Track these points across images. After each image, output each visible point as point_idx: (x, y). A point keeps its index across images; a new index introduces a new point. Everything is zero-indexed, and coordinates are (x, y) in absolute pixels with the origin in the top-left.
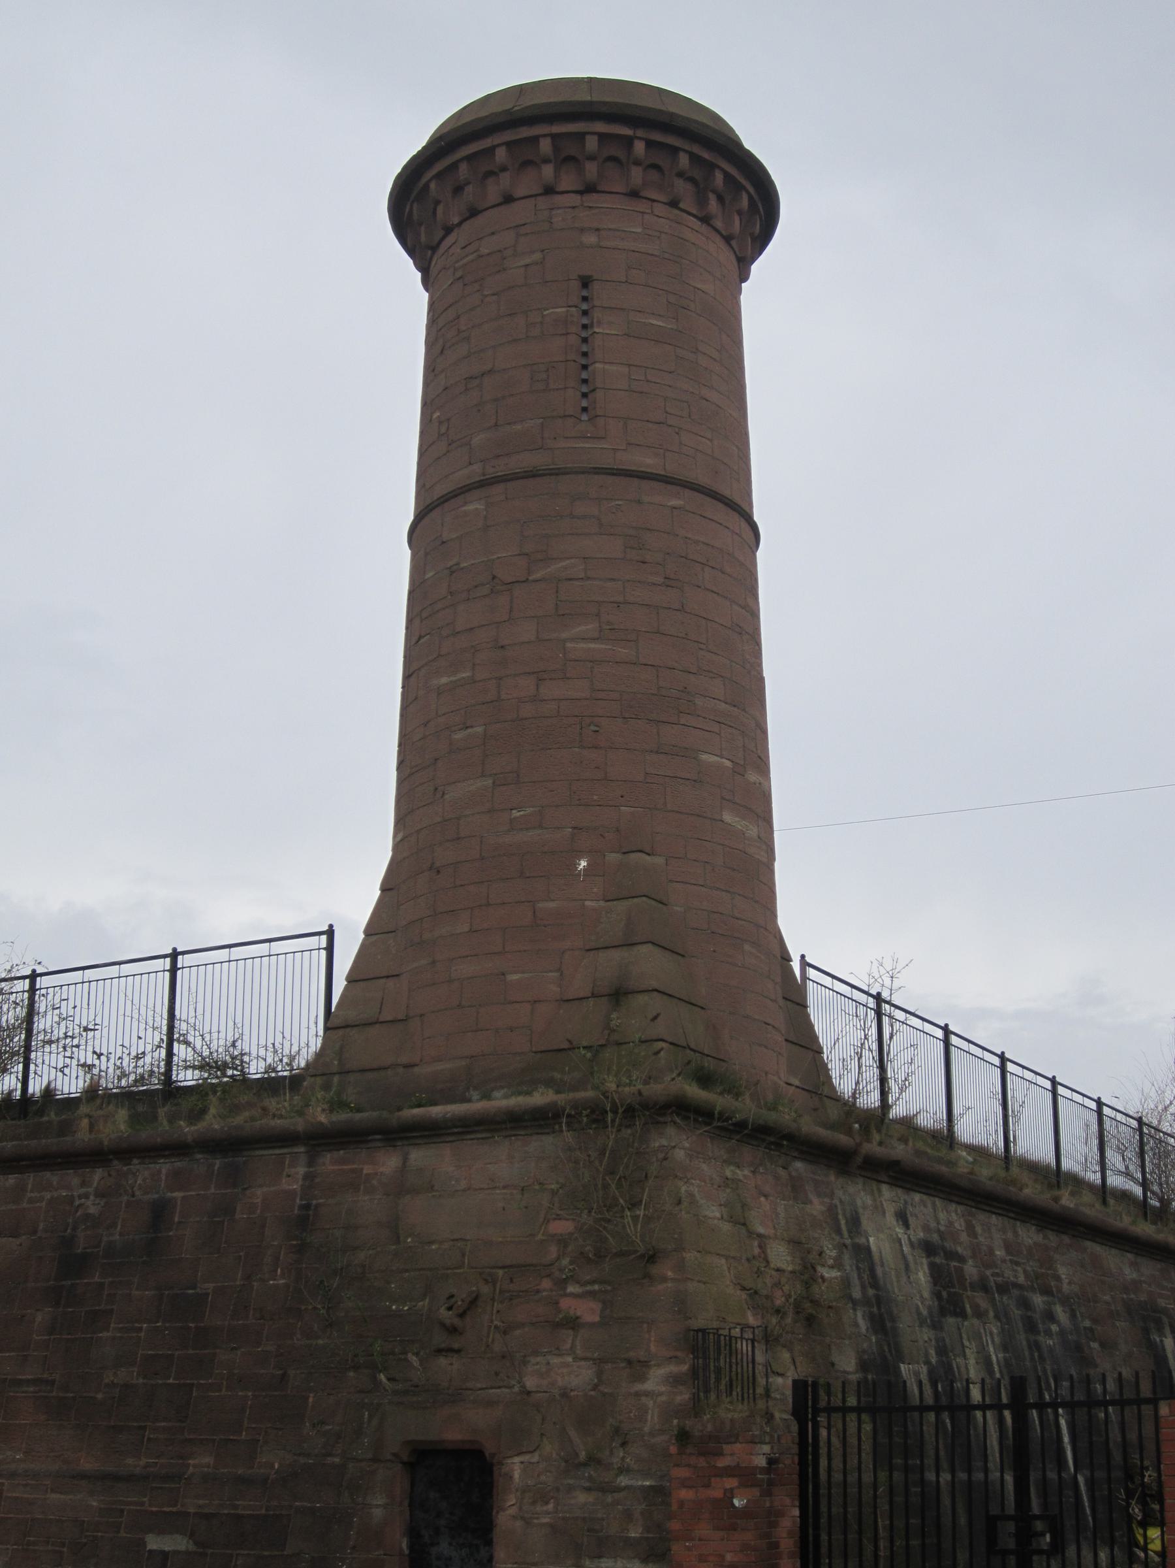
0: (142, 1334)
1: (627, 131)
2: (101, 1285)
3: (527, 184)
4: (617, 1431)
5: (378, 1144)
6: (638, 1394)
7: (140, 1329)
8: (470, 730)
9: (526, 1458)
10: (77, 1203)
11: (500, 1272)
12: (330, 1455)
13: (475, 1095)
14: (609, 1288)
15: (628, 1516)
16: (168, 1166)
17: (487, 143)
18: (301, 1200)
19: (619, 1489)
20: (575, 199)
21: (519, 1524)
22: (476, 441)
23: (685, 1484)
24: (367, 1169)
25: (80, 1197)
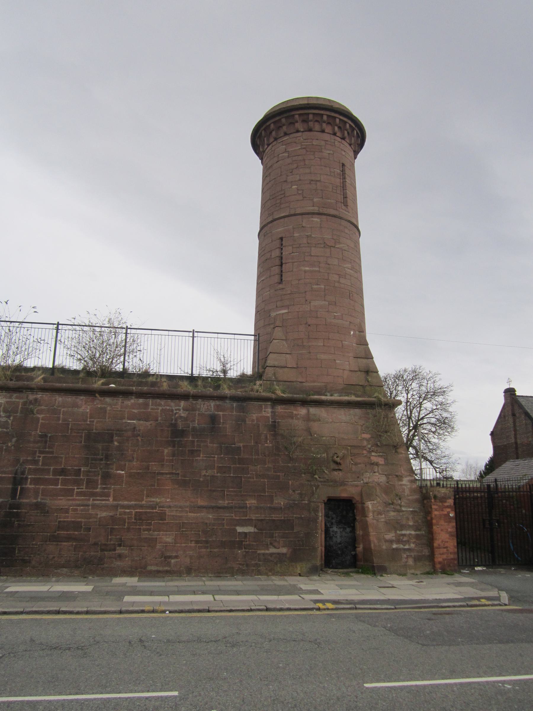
0: (216, 459)
1: (277, 118)
2: (193, 442)
3: (328, 129)
4: (397, 495)
5: (299, 405)
6: (401, 485)
7: (215, 457)
8: (319, 286)
9: (372, 502)
10: (175, 412)
11: (349, 448)
12: (304, 500)
13: (328, 394)
14: (385, 455)
15: (408, 519)
16: (214, 403)
17: (322, 112)
18: (272, 419)
19: (403, 511)
20: (340, 140)
21: (375, 521)
22: (315, 200)
23: (436, 510)
24: (295, 412)
25: (176, 410)
